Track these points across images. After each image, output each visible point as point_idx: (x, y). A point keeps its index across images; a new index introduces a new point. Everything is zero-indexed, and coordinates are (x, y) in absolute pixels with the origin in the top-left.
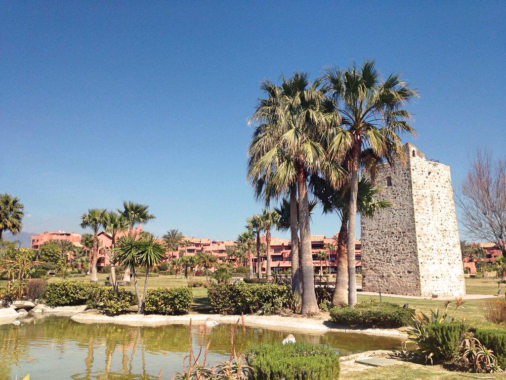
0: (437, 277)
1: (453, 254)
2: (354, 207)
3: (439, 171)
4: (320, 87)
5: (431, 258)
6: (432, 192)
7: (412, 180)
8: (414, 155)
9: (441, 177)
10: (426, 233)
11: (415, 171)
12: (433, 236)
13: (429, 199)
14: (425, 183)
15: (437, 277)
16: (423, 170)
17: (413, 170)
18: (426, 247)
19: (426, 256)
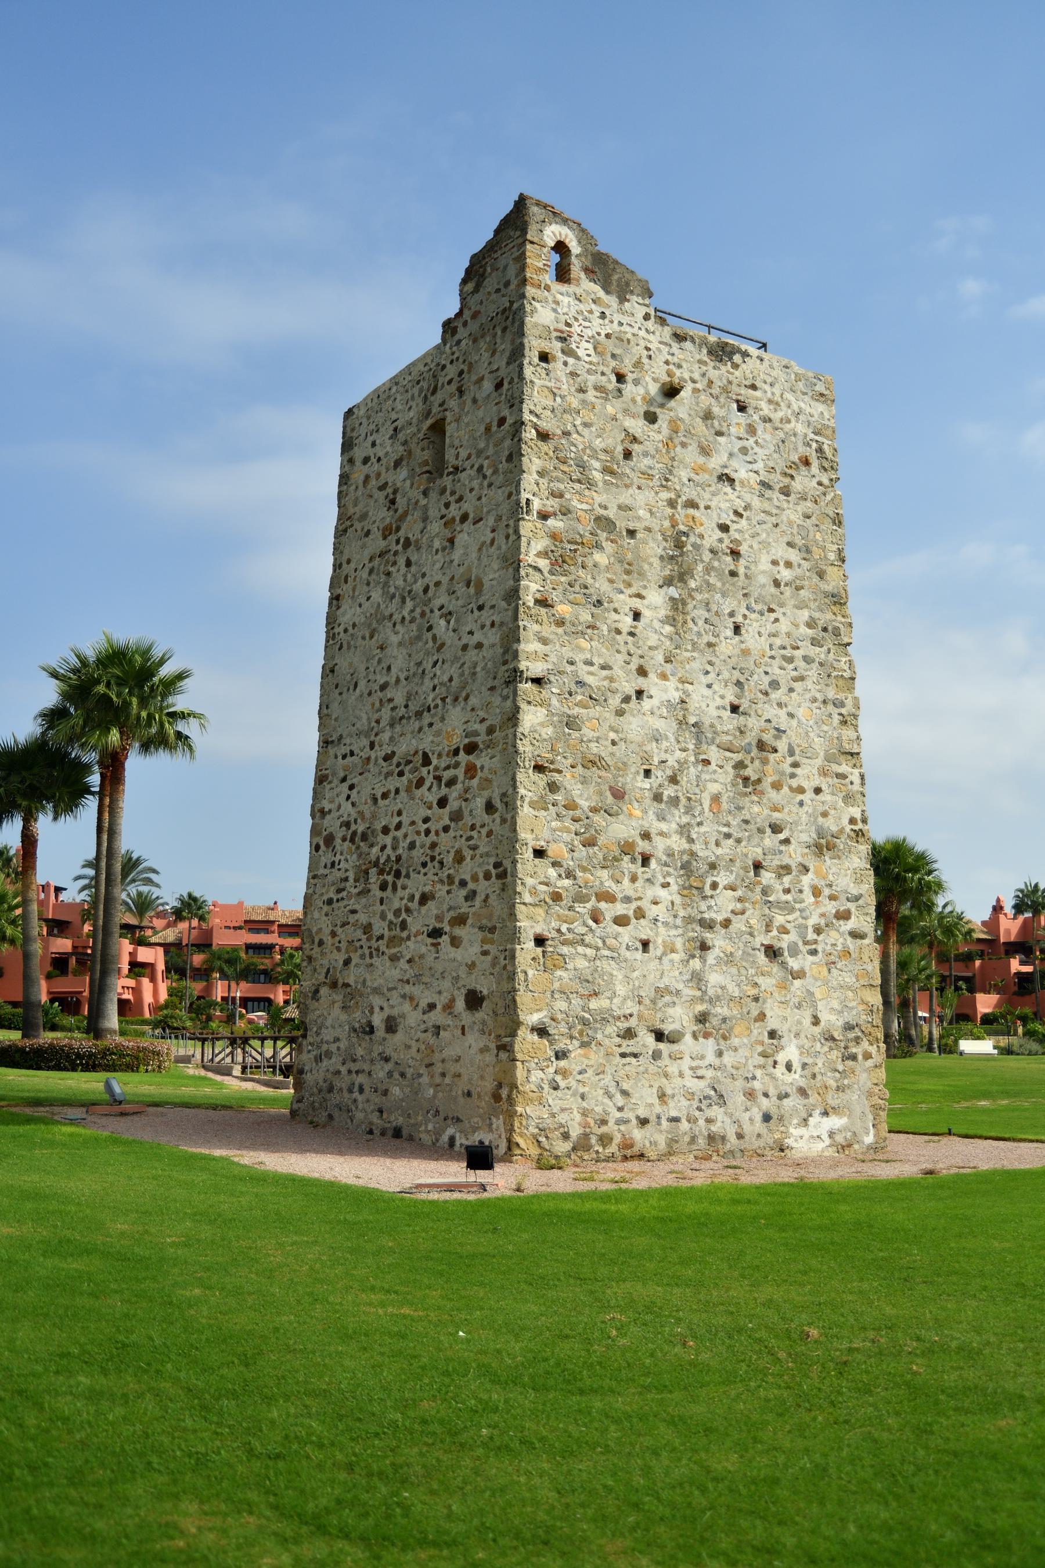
0: (660, 1036)
1: (796, 1065)
2: (130, 902)
3: (746, 394)
4: (345, 1091)
5: (628, 910)
6: (681, 513)
7: (527, 416)
8: (563, 274)
9: (764, 434)
10: (601, 749)
11: (557, 366)
12: (659, 776)
13: (653, 548)
14: (636, 448)
15: (660, 1036)
16: (626, 367)
17: (544, 357)
18: (589, 843)
19: (581, 898)
